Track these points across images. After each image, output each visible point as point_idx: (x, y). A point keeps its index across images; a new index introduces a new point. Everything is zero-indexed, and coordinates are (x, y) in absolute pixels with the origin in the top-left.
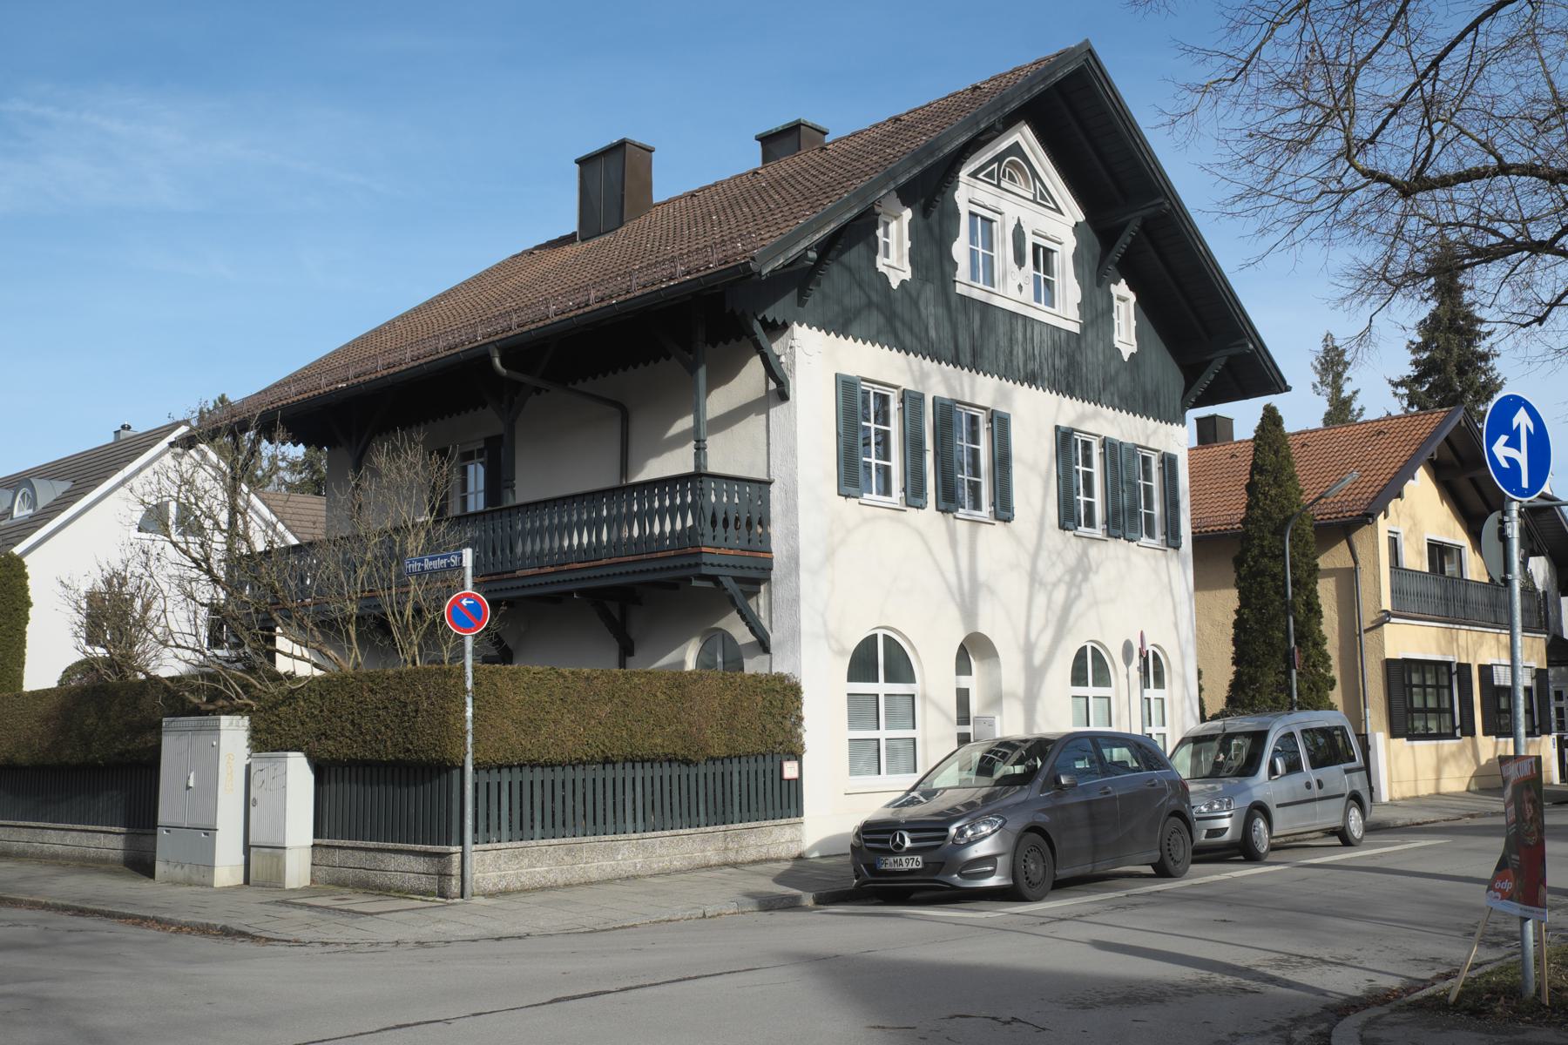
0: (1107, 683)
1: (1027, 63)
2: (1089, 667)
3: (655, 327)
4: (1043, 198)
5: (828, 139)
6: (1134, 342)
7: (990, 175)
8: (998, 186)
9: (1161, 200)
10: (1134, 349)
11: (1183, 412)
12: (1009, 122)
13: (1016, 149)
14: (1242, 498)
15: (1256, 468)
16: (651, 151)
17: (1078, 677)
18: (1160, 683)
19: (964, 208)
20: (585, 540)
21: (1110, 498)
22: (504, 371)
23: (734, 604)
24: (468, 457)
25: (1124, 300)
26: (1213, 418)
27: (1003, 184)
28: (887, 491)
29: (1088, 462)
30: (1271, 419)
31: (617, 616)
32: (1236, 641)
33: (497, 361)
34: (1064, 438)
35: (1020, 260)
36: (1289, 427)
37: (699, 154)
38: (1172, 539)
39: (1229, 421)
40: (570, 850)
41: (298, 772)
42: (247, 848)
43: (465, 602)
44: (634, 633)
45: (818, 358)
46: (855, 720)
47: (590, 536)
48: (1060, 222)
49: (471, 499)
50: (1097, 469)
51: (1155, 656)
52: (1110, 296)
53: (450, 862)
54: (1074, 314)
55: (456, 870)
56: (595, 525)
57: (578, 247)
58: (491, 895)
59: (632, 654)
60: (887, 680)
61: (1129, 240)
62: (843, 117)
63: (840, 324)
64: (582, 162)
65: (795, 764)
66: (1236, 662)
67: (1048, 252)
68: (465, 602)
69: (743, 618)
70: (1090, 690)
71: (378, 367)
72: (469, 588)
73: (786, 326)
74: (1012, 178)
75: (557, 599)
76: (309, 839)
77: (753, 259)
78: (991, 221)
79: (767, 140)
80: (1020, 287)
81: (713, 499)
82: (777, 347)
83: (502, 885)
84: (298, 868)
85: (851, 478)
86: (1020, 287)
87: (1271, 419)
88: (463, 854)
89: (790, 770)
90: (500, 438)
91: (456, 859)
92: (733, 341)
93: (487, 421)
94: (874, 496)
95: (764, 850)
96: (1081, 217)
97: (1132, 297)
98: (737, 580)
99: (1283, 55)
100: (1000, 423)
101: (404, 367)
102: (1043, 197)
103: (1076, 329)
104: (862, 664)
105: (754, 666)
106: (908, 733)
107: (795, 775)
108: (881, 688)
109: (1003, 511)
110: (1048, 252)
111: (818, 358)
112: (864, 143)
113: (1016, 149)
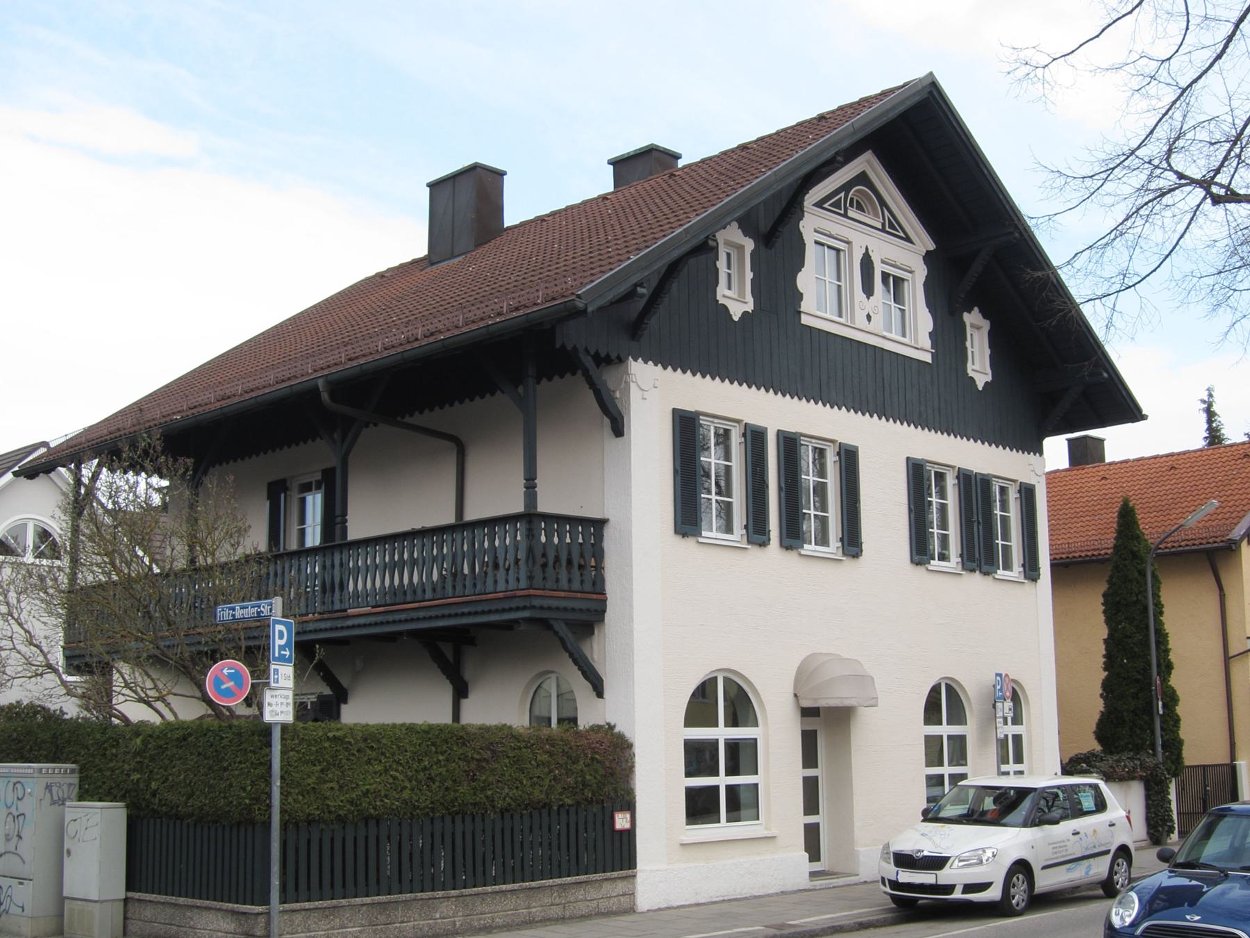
4: (892, 227)
6: (989, 371)
8: (845, 215)
9: (1011, 230)
10: (989, 378)
12: (851, 153)
17: (932, 712)
19: (809, 236)
20: (416, 579)
21: (974, 529)
24: (307, 488)
25: (978, 328)
27: (851, 213)
28: (729, 529)
31: (451, 659)
34: (918, 474)
35: (868, 290)
38: (1031, 570)
39: (1101, 441)
44: (468, 674)
45: (655, 393)
46: (692, 769)
48: (909, 255)
49: (309, 532)
54: (927, 343)
59: (466, 696)
62: (702, 131)
64: (434, 186)
67: (898, 281)
69: (576, 662)
71: (240, 390)
73: (621, 360)
75: (392, 637)
77: (579, 296)
78: (838, 251)
80: (869, 317)
81: (543, 539)
85: (688, 519)
86: (869, 317)
88: (268, 914)
89: (622, 821)
90: (333, 470)
92: (556, 378)
93: (317, 454)
94: (714, 534)
95: (594, 904)
96: (931, 246)
97: (986, 325)
98: (569, 623)
100: (849, 458)
101: (236, 400)
102: (891, 226)
103: (928, 358)
104: (701, 705)
107: (627, 826)
109: (852, 543)
110: (898, 281)
111: (655, 393)
113: (862, 179)
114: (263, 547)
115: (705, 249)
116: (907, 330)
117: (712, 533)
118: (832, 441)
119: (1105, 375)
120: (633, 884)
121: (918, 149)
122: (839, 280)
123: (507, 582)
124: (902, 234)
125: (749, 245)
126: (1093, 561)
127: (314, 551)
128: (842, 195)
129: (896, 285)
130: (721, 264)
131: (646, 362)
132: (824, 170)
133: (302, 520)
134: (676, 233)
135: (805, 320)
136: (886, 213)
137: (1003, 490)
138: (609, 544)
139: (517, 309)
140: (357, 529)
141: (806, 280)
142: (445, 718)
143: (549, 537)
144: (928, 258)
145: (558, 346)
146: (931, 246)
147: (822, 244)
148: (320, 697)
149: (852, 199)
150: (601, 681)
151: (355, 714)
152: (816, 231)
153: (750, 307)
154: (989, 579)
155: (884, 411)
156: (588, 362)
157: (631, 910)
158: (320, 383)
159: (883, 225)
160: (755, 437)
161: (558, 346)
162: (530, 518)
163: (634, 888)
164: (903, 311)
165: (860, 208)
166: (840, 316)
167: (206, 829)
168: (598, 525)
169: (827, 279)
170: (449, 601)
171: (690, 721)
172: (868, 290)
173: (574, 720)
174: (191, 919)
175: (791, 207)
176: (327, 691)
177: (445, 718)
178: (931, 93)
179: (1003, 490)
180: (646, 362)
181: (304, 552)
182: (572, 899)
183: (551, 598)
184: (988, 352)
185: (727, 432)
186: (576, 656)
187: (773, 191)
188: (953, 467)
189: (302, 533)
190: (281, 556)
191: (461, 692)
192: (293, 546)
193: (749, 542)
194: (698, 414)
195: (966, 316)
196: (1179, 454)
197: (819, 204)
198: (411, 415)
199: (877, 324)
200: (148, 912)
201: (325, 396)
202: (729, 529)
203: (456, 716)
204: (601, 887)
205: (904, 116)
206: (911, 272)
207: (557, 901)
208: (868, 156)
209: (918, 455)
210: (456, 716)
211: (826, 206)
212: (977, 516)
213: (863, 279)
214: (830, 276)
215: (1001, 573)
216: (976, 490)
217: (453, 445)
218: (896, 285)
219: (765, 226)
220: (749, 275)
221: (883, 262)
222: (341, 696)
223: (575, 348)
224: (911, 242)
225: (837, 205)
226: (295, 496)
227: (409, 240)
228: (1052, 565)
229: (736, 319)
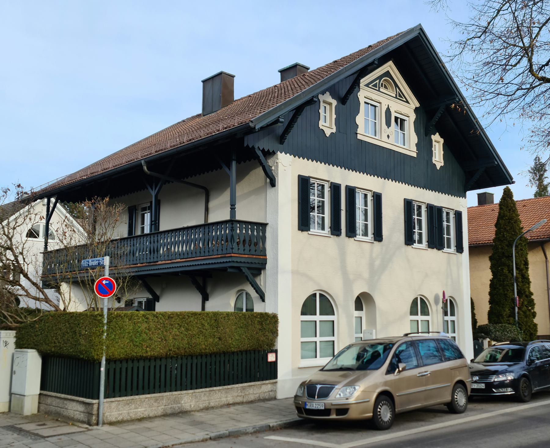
0: (428, 314)
1: (393, 35)
2: (419, 306)
3: (219, 151)
4: (400, 96)
5: (309, 71)
6: (442, 161)
7: (375, 86)
8: (379, 91)
10: (443, 164)
11: (465, 193)
12: (383, 61)
13: (387, 74)
14: (494, 229)
15: (501, 217)
16: (233, 77)
17: (413, 311)
18: (453, 314)
19: (362, 100)
21: (435, 231)
22: (149, 172)
23: (248, 280)
24: (144, 209)
25: (438, 142)
26: (485, 194)
27: (381, 90)
28: (323, 229)
29: (419, 214)
30: (508, 194)
31: (201, 284)
32: (490, 294)
33: (145, 168)
34: (408, 205)
35: (388, 124)
36: (515, 198)
37: (255, 78)
38: (460, 249)
39: (492, 195)
40: (157, 400)
41: (32, 361)
42: (11, 394)
43: (104, 282)
44: (209, 290)
45: (289, 167)
47: (186, 247)
48: (408, 108)
50: (424, 218)
51: (451, 302)
52: (431, 140)
53: (92, 408)
54: (414, 149)
55: (95, 412)
56: (188, 242)
57: (202, 118)
58: (111, 424)
59: (208, 300)
60: (320, 314)
61: (440, 115)
62: (316, 60)
63: (299, 152)
64: (204, 82)
65: (274, 355)
66: (490, 302)
67: (402, 121)
68: (104, 282)
69: (252, 286)
70: (420, 318)
72: (107, 276)
73: (274, 153)
74: (386, 87)
76: (37, 391)
77: (252, 122)
78: (375, 106)
79: (282, 72)
80: (388, 136)
81: (238, 231)
82: (270, 162)
83: (120, 418)
84: (30, 406)
85: (304, 224)
86: (388, 136)
87: (508, 194)
88: (99, 403)
89: (271, 358)
91: (95, 407)
94: (316, 230)
95: (257, 395)
96: (418, 105)
97: (442, 141)
99: (503, 23)
100: (378, 198)
102: (400, 96)
103: (415, 155)
104: (308, 307)
105: (258, 308)
106: (331, 338)
107: (274, 360)
108: (318, 318)
109: (378, 236)
110: (402, 121)
111: (289, 167)
112: (321, 71)
113: (387, 74)
114: (126, 235)
115: (312, 102)
116: (407, 143)
117: (315, 229)
118: (371, 191)
119: (496, 163)
120: (276, 386)
121: (414, 59)
122: (375, 120)
123: (222, 250)
124: (404, 100)
125: (334, 103)
126: (480, 246)
127: (147, 235)
128: (378, 81)
129: (400, 123)
130: (321, 111)
131: (286, 154)
132: (369, 68)
133: (143, 223)
134: (299, 94)
135: (359, 137)
136: (398, 90)
137: (448, 214)
138: (268, 234)
139: (226, 128)
140: (163, 227)
141: (360, 119)
142: (198, 309)
143: (252, 232)
144: (416, 110)
145: (245, 145)
146: (418, 105)
147: (368, 104)
148: (148, 299)
149: (382, 84)
150: (264, 295)
151: (161, 307)
152: (365, 97)
153: (334, 131)
154: (440, 252)
155: (395, 178)
156: (260, 154)
157: (275, 399)
158: (143, 162)
159: (396, 95)
160: (335, 188)
161: (245, 145)
162: (232, 222)
163: (276, 388)
164: (404, 134)
165: (386, 87)
166: (375, 136)
167: (74, 362)
168: (263, 226)
169: (370, 119)
170: (198, 258)
171: (303, 313)
172: (388, 124)
173: (253, 310)
174: (66, 404)
175: (355, 85)
176: (151, 297)
177: (198, 309)
178: (419, 33)
179: (448, 214)
180: (286, 154)
181: (143, 235)
182: (247, 393)
183: (240, 259)
184: (442, 152)
185: (323, 186)
186: (253, 283)
187: (345, 81)
188: (425, 203)
189: (143, 229)
190: (134, 237)
191: (205, 298)
192: (139, 233)
193: (332, 234)
194: (310, 177)
195: (433, 136)
196: (528, 200)
197: (367, 85)
198: (187, 178)
199: (392, 140)
200: (49, 400)
201: (145, 168)
202: (323, 229)
203: (203, 308)
204: (261, 387)
205: (406, 44)
206: (408, 117)
207: (240, 394)
208: (390, 63)
209: (409, 197)
210: (203, 308)
211: (370, 86)
212: (436, 224)
213: (387, 115)
214: (371, 119)
215: (446, 250)
216: (435, 213)
217: (201, 190)
218: (400, 123)
219: (343, 93)
220: (334, 116)
221: (395, 112)
222: (157, 298)
223: (253, 147)
224: (409, 103)
225: (375, 86)
226: (140, 213)
227: (196, 107)
228: (469, 247)
229: (328, 136)
